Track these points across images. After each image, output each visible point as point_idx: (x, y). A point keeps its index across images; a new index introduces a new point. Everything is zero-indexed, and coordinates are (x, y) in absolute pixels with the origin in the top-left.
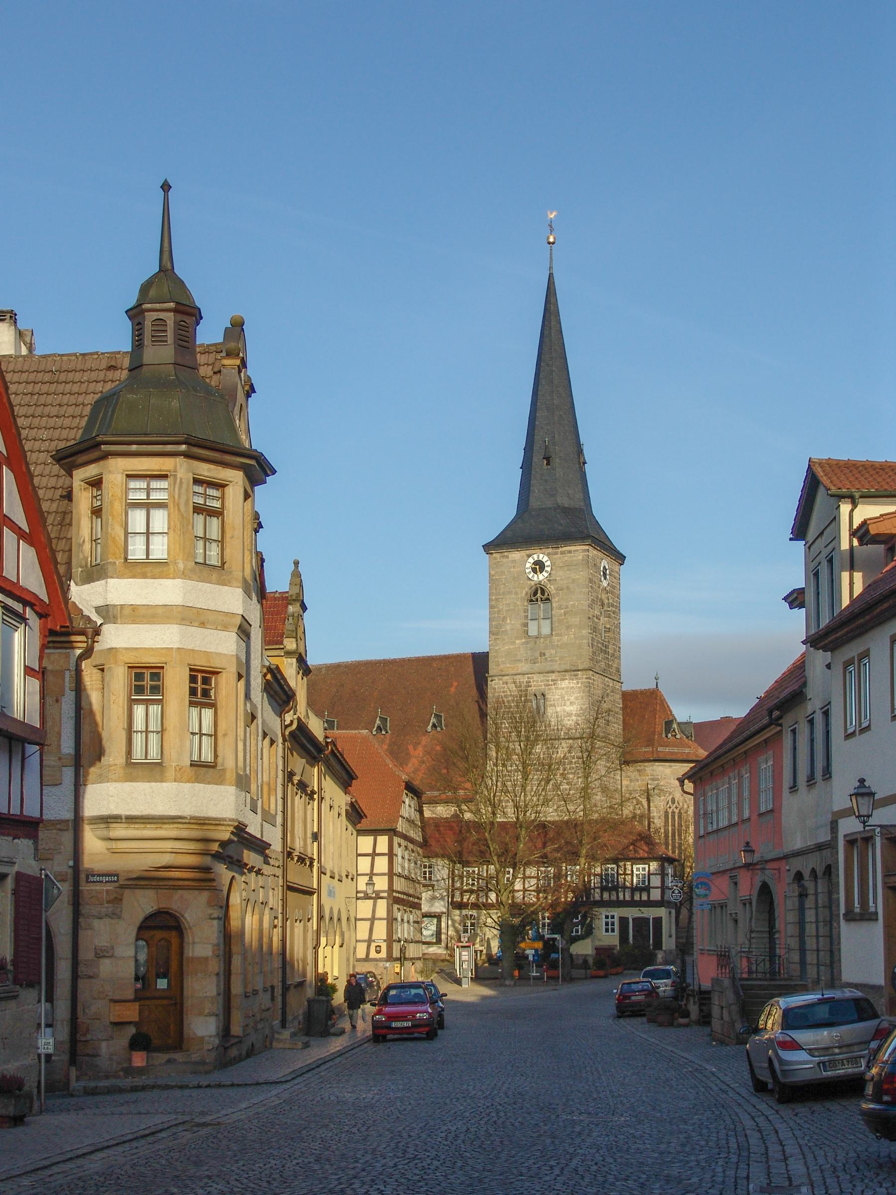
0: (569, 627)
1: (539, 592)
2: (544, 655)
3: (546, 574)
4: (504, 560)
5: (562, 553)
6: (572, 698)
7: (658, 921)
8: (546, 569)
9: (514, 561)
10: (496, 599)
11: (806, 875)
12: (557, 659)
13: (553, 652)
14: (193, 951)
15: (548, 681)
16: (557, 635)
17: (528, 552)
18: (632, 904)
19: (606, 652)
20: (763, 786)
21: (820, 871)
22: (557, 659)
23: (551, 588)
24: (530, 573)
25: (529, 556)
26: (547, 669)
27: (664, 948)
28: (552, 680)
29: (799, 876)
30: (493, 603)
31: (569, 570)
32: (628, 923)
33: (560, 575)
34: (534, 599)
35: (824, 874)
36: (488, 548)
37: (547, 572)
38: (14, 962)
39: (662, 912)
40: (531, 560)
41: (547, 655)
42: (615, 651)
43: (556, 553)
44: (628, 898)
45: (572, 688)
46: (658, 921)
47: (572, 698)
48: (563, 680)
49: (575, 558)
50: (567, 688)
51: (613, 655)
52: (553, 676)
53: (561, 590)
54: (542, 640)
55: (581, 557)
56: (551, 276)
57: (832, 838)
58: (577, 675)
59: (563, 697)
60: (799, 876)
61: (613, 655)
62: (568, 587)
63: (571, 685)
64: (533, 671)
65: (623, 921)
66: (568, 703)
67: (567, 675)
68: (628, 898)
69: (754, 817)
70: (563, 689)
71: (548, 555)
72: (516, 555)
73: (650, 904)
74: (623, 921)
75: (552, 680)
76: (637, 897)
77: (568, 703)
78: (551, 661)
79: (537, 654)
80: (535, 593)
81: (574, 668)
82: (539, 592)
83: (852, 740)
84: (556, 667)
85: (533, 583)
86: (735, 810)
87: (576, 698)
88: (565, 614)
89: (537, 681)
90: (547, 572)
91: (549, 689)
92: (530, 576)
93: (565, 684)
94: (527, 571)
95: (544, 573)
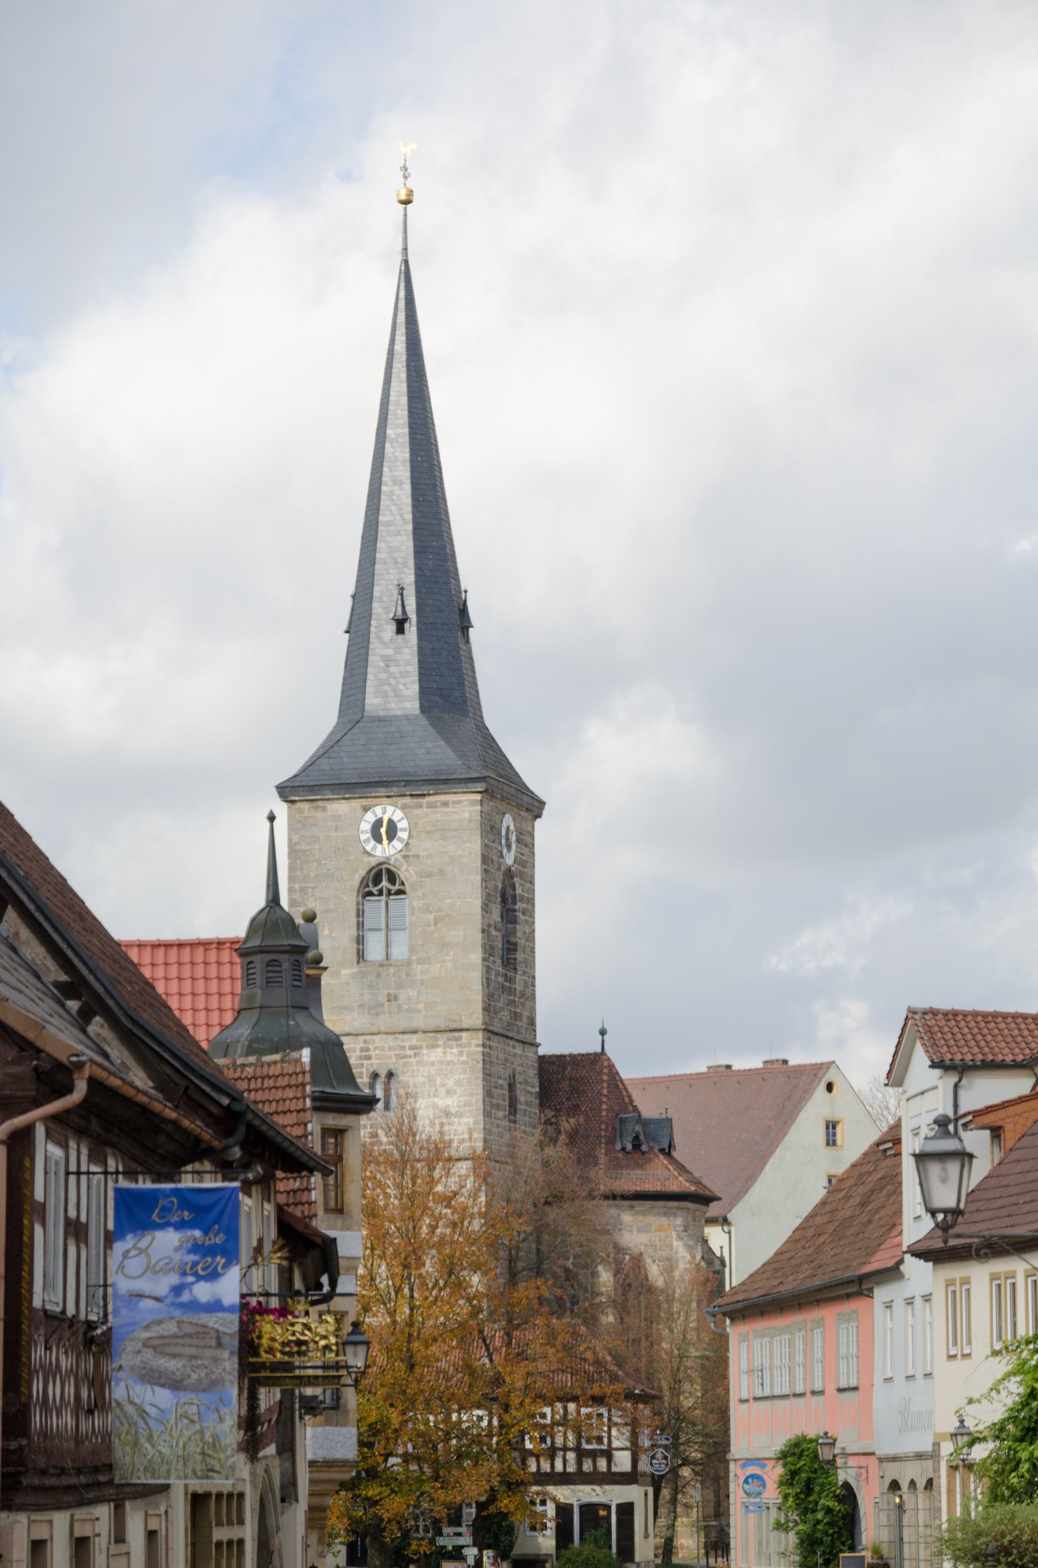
0: (444, 947)
1: (384, 878)
2: (396, 998)
3: (397, 845)
4: (319, 815)
5: (431, 806)
6: (451, 1083)
7: (626, 1510)
8: (400, 834)
9: (337, 817)
10: (303, 890)
11: (904, 1485)
12: (421, 1006)
13: (413, 993)
14: (787, 1540)
15: (403, 1048)
16: (421, 961)
17: (364, 802)
18: (579, 1478)
19: (511, 991)
20: (843, 1351)
21: (921, 1484)
22: (421, 1006)
23: (406, 873)
24: (367, 841)
25: (366, 809)
26: (403, 1025)
27: (637, 1559)
28: (411, 1048)
29: (895, 1486)
30: (297, 896)
31: (444, 838)
32: (572, 1512)
33: (424, 847)
34: (375, 890)
35: (926, 1488)
36: (287, 791)
37: (401, 840)
38: (211, 1527)
39: (634, 1494)
40: (370, 818)
41: (402, 997)
42: (526, 986)
43: (420, 806)
44: (571, 1468)
45: (449, 1063)
46: (626, 1510)
47: (451, 1083)
48: (433, 1047)
49: (455, 817)
50: (441, 1062)
51: (522, 995)
52: (413, 1040)
53: (429, 875)
54: (392, 970)
55: (466, 815)
56: (406, 262)
57: (934, 1450)
58: (460, 1038)
59: (431, 1079)
60: (895, 1486)
61: (522, 995)
62: (441, 872)
63: (449, 1058)
64: (374, 1030)
65: (564, 1511)
66: (442, 1091)
67: (441, 1039)
68: (571, 1468)
69: (830, 1390)
70: (432, 1064)
71: (403, 808)
72: (341, 808)
73: (613, 1478)
74: (564, 1511)
75: (411, 1048)
76: (587, 1466)
77: (442, 1091)
78: (409, 1010)
79: (382, 998)
80: (377, 880)
81: (453, 1026)
82: (384, 878)
83: (952, 1364)
84: (418, 1022)
85: (373, 862)
86: (799, 1373)
87: (458, 1083)
88: (436, 922)
89: (382, 1049)
90: (401, 840)
91: (405, 1065)
92: (369, 848)
93: (435, 1055)
94: (363, 837)
95: (395, 842)
